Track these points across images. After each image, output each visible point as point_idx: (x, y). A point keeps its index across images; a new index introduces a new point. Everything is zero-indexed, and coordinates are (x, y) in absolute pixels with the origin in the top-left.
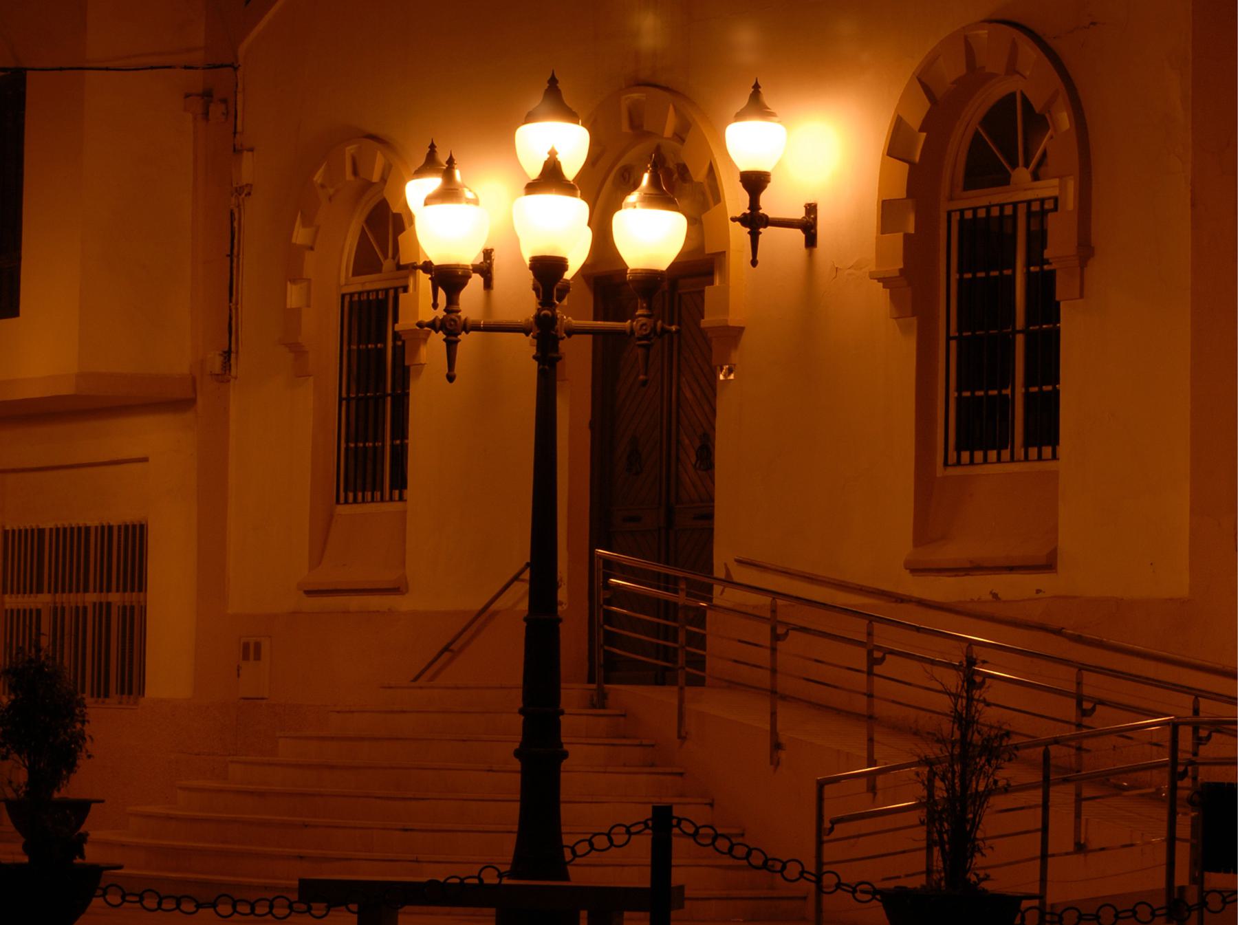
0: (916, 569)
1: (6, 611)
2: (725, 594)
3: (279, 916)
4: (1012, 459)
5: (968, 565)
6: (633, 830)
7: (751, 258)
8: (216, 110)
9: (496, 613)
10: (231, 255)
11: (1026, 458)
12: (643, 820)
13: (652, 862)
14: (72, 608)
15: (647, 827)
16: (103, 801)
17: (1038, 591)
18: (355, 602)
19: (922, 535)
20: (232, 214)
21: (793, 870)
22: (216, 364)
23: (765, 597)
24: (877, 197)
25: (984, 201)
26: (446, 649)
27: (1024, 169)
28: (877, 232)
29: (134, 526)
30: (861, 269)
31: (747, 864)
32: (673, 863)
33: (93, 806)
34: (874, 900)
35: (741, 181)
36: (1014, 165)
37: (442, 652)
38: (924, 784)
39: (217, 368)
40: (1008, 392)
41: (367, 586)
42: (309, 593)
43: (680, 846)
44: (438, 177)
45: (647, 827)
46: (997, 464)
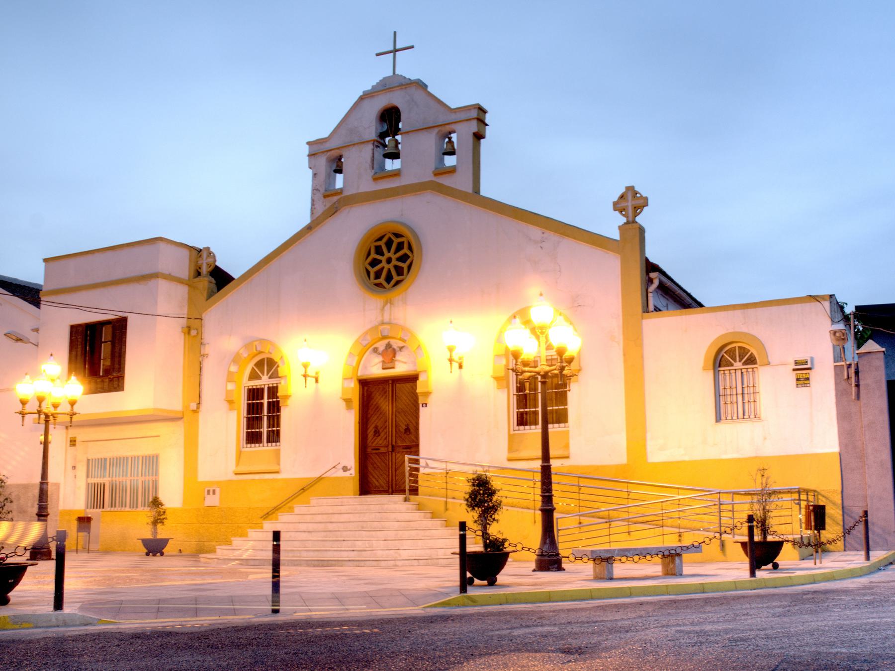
0: (509, 460)
1: (89, 484)
4: (263, 446)
6: (683, 548)
8: (193, 332)
10: (200, 375)
11: (268, 446)
12: (52, 536)
14: (120, 482)
15: (54, 540)
17: (562, 464)
18: (257, 477)
19: (511, 449)
20: (200, 363)
21: (572, 558)
22: (193, 406)
24: (752, 309)
26: (303, 489)
29: (150, 457)
32: (458, 556)
33: (170, 540)
37: (301, 490)
39: (195, 408)
40: (262, 430)
41: (518, 458)
42: (236, 474)
44: (83, 383)
45: (54, 540)
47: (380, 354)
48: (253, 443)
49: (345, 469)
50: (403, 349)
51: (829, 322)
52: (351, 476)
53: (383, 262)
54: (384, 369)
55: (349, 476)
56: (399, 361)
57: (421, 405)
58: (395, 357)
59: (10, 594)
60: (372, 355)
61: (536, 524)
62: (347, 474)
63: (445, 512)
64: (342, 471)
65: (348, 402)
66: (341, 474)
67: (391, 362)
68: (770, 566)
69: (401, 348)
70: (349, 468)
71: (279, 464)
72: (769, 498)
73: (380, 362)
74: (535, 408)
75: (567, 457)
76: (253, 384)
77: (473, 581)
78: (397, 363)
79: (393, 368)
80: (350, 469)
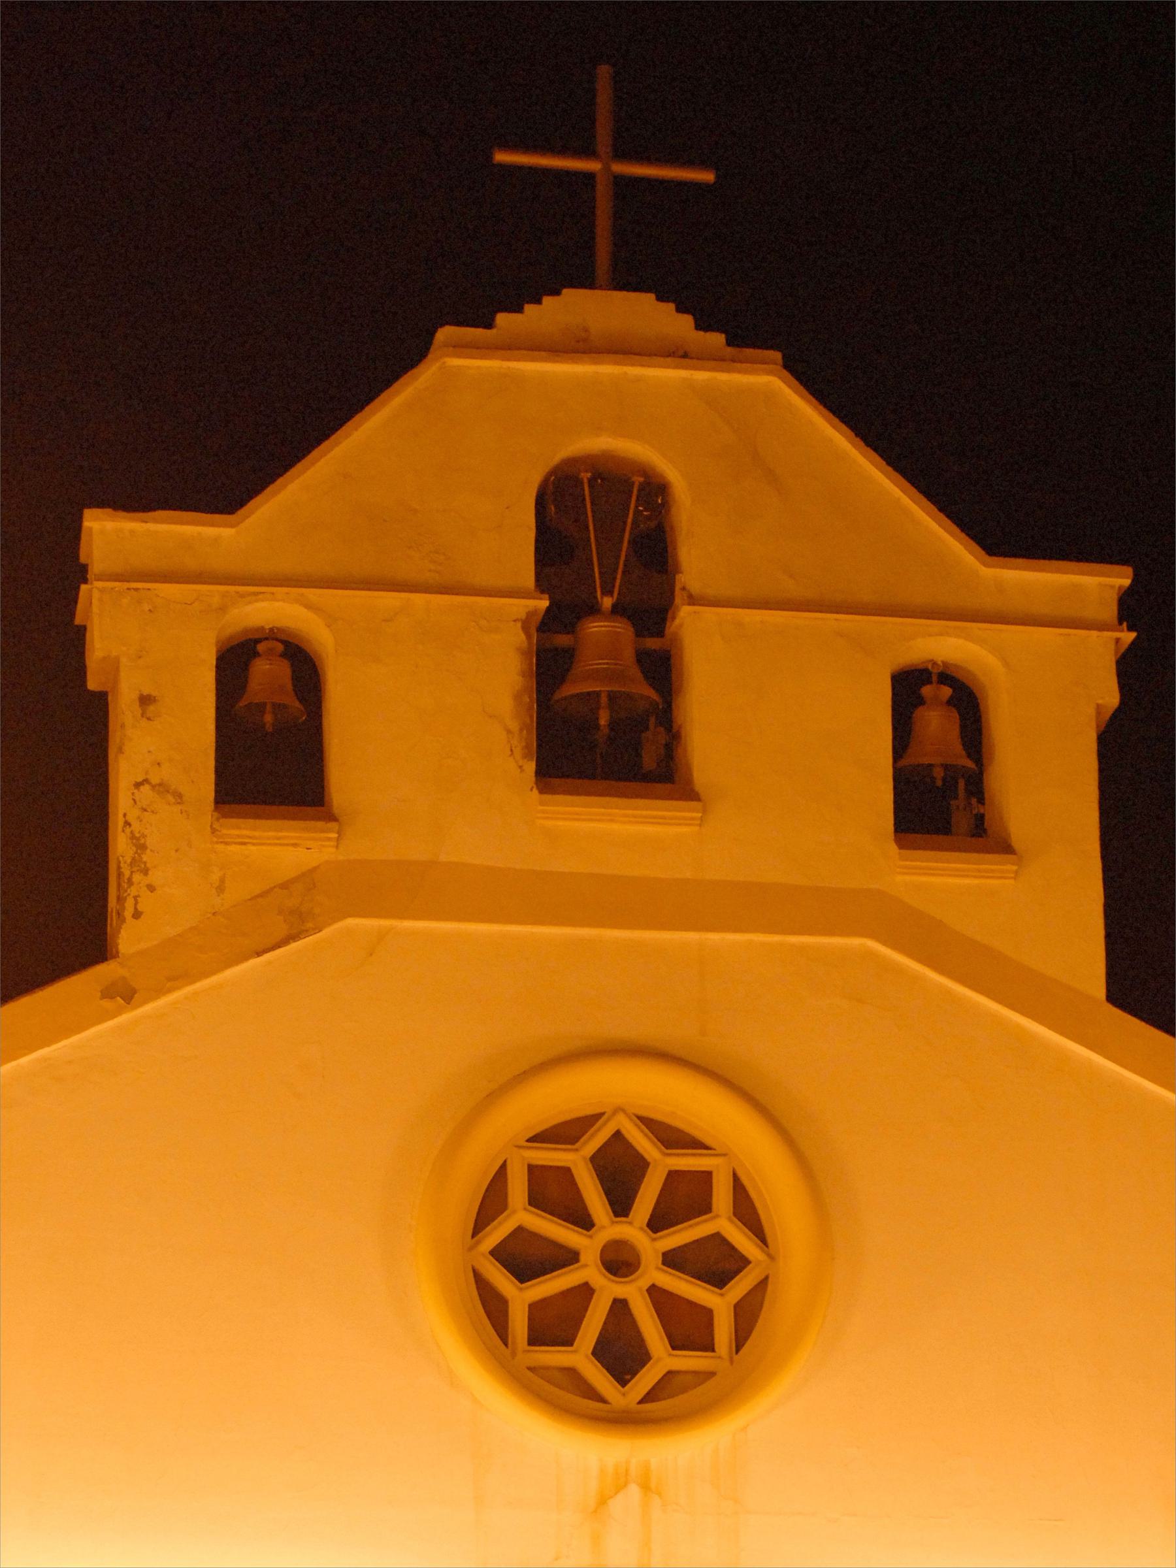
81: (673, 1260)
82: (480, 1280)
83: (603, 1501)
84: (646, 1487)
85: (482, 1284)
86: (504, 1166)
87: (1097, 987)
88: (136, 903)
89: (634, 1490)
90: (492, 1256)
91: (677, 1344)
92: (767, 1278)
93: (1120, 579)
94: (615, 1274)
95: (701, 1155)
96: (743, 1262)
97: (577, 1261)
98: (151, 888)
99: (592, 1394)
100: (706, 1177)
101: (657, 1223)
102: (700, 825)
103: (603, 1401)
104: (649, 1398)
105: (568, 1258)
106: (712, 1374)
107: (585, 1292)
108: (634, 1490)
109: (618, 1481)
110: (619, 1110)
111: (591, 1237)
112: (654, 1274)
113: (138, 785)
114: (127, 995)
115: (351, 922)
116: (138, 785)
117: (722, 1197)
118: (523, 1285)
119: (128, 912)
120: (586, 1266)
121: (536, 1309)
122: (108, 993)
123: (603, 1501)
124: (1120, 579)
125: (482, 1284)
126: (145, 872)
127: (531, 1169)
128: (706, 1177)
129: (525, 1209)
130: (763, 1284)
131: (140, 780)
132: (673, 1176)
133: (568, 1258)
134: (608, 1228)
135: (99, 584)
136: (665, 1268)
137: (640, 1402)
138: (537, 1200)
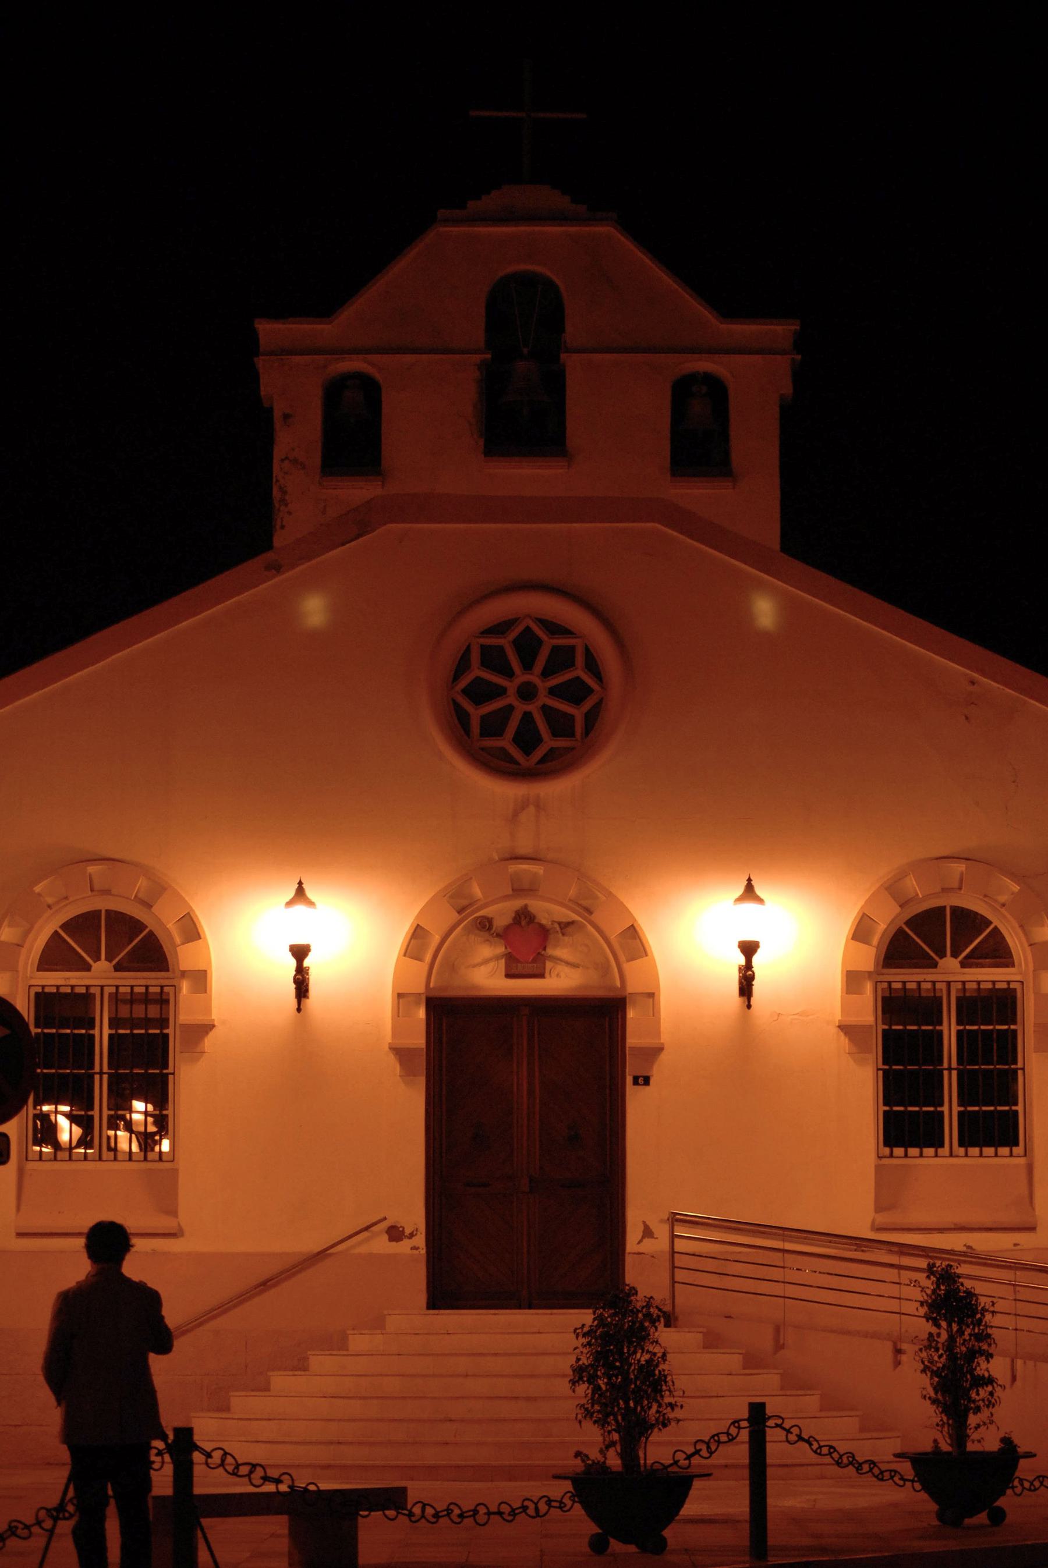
2: (642, 1244)
3: (391, 1517)
5: (953, 1227)
7: (297, 1007)
9: (331, 1255)
13: (765, 1446)
16: (1035, 1455)
17: (1015, 1245)
23: (79, 1239)
25: (920, 978)
27: (953, 959)
28: (842, 993)
30: (808, 1016)
31: (820, 1442)
34: (861, 1462)
35: (290, 951)
36: (942, 955)
38: (996, 1383)
42: (20, 1235)
43: (773, 1436)
46: (920, 1158)
47: (498, 935)
48: (989, 1145)
49: (395, 1234)
50: (569, 929)
51: (954, 960)
52: (415, 1252)
53: (540, 703)
54: (508, 976)
55: (408, 1251)
56: (557, 960)
57: (629, 1080)
58: (545, 949)
59: (667, 1533)
60: (472, 937)
61: (1006, 1390)
62: (403, 1247)
63: (775, 1352)
64: (386, 1237)
65: (401, 1053)
66: (381, 1245)
67: (534, 961)
68: (982, 1518)
69: (565, 926)
70: (407, 1232)
71: (174, 1213)
72: (988, 1362)
73: (497, 958)
74: (935, 1106)
75: (1032, 1229)
76: (73, 982)
77: (607, 1544)
78: (549, 965)
79: (541, 976)
80: (411, 1235)
81: (553, 692)
82: (456, 704)
83: (516, 814)
84: (537, 806)
85: (457, 706)
86: (469, 646)
87: (777, 547)
88: (282, 520)
89: (532, 809)
90: (524, 630)
91: (555, 734)
92: (602, 698)
93: (794, 326)
94: (526, 700)
95: (570, 638)
96: (590, 691)
97: (505, 694)
98: (290, 513)
99: (512, 760)
100: (572, 649)
101: (546, 674)
102: (568, 469)
103: (519, 764)
104: (542, 761)
105: (501, 691)
106: (573, 749)
107: (510, 708)
108: (532, 809)
109: (522, 805)
110: (528, 616)
111: (511, 681)
112: (544, 699)
113: (282, 460)
114: (277, 568)
115: (391, 525)
116: (282, 460)
117: (580, 659)
118: (478, 707)
119: (278, 527)
120: (509, 696)
121: (484, 719)
122: (269, 567)
123: (516, 814)
124: (794, 326)
125: (457, 706)
126: (286, 505)
127: (483, 647)
128: (572, 649)
129: (479, 668)
130: (601, 701)
131: (283, 457)
132: (555, 649)
133: (501, 691)
134: (512, 686)
135: (263, 357)
136: (512, 743)
137: (536, 764)
138: (485, 663)
